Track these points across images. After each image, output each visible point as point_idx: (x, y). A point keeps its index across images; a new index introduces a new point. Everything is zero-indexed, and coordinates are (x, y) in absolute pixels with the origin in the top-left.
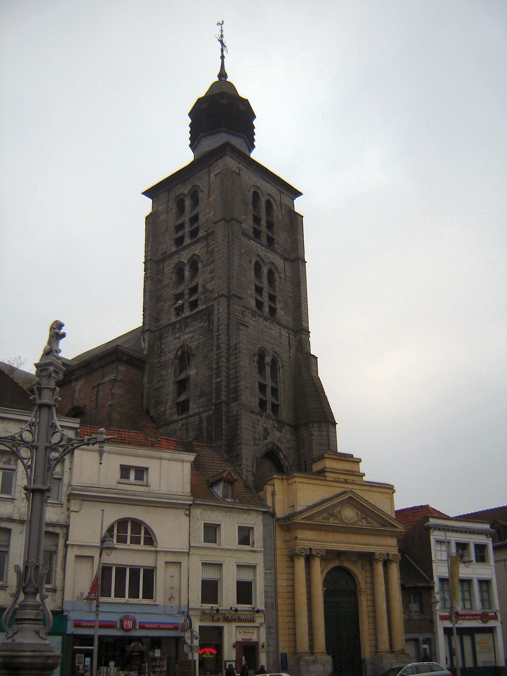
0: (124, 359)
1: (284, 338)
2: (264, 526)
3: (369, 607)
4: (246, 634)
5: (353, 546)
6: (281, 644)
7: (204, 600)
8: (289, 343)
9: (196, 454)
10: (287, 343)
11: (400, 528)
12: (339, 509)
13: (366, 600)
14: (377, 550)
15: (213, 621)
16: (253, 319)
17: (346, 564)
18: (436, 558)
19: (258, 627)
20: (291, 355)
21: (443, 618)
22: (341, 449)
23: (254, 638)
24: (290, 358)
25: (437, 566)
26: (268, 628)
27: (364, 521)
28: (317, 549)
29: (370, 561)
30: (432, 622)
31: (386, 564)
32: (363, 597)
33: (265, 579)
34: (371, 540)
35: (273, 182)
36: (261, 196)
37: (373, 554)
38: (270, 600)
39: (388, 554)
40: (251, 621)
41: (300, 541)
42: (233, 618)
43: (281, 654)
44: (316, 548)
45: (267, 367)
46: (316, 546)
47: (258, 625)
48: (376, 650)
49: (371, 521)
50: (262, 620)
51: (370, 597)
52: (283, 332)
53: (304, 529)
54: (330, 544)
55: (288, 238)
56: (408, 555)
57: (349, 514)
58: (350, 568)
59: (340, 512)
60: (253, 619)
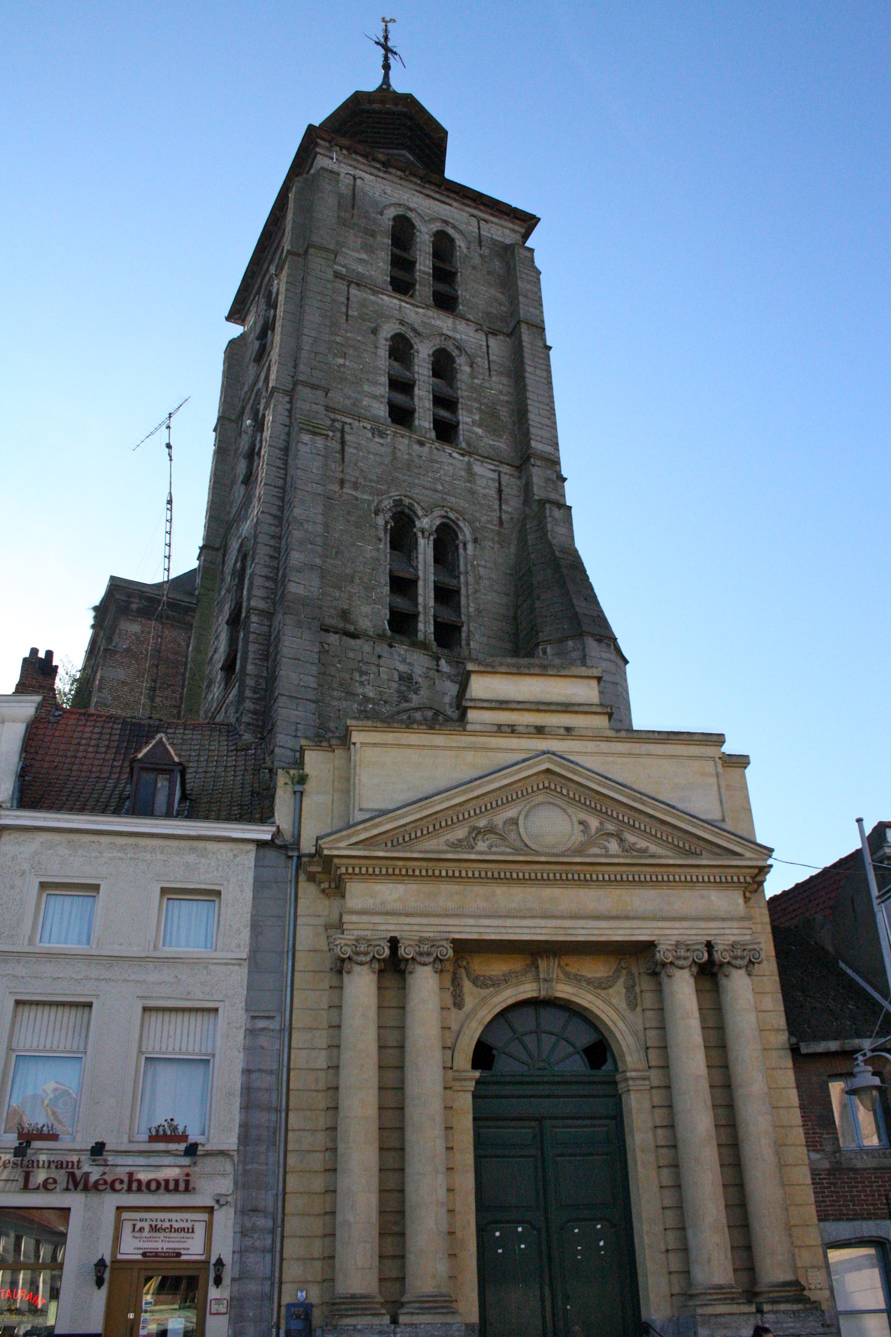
0: (134, 606)
1: (481, 482)
2: (259, 885)
3: (660, 1131)
4: (161, 1235)
5: (567, 923)
6: (292, 1271)
8: (500, 491)
9: (38, 698)
10: (493, 493)
11: (748, 854)
12: (511, 813)
13: (647, 1105)
14: (666, 935)
15: (26, 1187)
16: (377, 439)
19: (210, 1210)
20: (504, 516)
23: (193, 1248)
24: (501, 523)
26: (247, 1210)
27: (613, 846)
28: (422, 941)
29: (655, 974)
31: (709, 972)
32: (633, 1096)
33: (250, 1050)
34: (643, 899)
35: (455, 200)
36: (417, 222)
37: (651, 946)
38: (263, 1118)
39: (709, 945)
40: (176, 1190)
41: (355, 918)
42: (109, 1178)
43: (289, 1306)
44: (416, 936)
45: (421, 541)
47: (209, 1202)
48: (687, 1294)
49: (642, 844)
50: (225, 1185)
51: (658, 1097)
52: (478, 469)
53: (373, 876)
54: (471, 921)
55: (499, 295)
56: (847, 963)
57: (553, 827)
59: (514, 822)
60: (187, 1182)
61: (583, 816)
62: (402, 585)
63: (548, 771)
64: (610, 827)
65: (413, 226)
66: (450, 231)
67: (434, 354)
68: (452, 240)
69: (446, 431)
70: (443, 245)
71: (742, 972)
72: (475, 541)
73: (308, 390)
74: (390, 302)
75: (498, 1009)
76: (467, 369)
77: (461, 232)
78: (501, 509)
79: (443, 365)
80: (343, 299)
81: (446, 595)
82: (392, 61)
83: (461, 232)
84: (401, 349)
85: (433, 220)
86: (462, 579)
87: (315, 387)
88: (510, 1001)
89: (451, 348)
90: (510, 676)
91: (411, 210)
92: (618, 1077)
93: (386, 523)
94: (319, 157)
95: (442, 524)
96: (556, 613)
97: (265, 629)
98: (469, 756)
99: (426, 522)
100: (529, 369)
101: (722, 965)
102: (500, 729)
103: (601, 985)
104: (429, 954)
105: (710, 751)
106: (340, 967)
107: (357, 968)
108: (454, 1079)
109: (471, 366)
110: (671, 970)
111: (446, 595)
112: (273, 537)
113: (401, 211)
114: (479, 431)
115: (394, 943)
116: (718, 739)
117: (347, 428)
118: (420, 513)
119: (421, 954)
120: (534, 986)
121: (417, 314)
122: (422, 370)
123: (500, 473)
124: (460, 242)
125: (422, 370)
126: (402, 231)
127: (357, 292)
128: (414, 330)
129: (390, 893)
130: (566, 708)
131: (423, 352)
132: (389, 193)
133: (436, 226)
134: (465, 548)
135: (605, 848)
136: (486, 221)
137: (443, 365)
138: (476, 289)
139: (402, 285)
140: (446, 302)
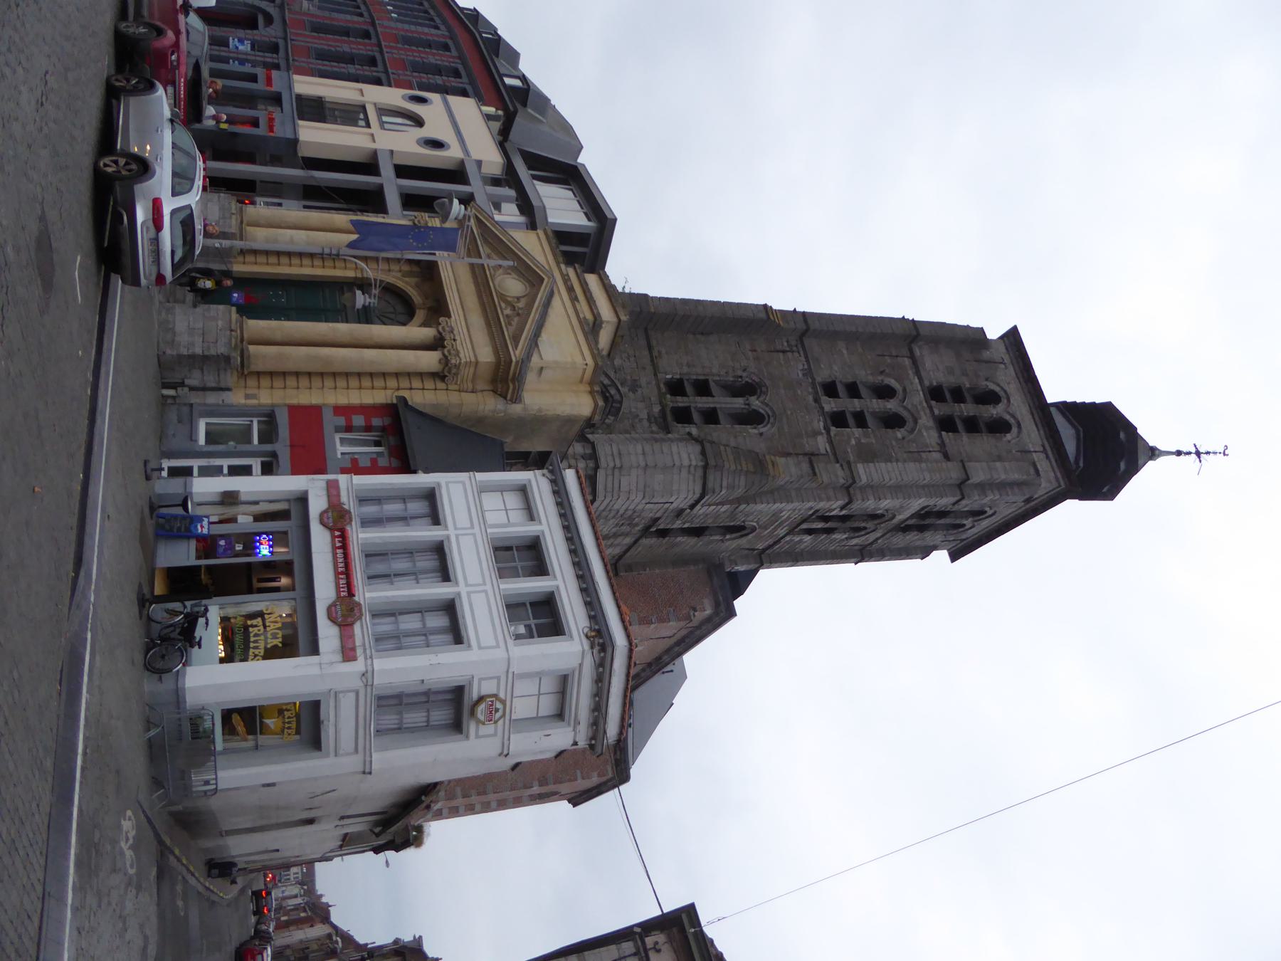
69: (838, 420)
76: (899, 435)
99: (755, 403)
124: (1009, 436)
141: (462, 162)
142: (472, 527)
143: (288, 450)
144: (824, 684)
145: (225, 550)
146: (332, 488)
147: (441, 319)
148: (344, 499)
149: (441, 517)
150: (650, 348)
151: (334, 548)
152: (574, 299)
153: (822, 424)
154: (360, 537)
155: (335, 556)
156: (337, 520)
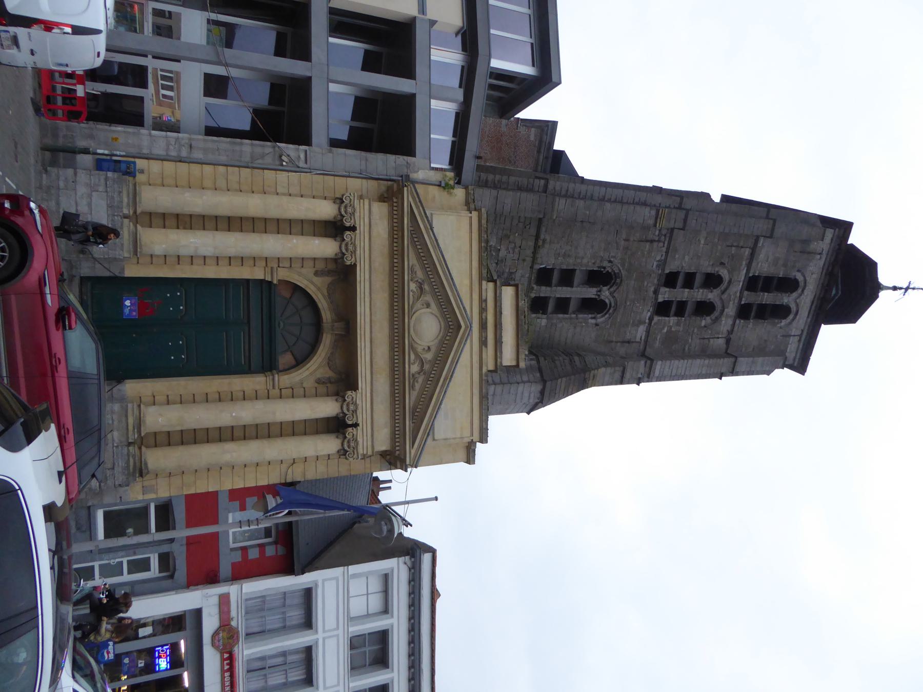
7: (191, 499)
11: (413, 451)
13: (258, 387)
17: (327, 340)
18: (355, 576)
21: (224, 601)
22: (495, 422)
25: (337, 579)
30: (212, 579)
31: (337, 426)
34: (383, 385)
36: (795, 295)
37: (355, 388)
39: (356, 425)
41: (367, 207)
46: (361, 240)
49: (417, 386)
58: (315, 358)
59: (428, 306)
61: (433, 349)
62: (567, 277)
63: (460, 327)
64: (427, 367)
65: (792, 292)
66: (791, 317)
67: (711, 303)
68: (785, 317)
69: (662, 309)
70: (781, 312)
71: (340, 447)
72: (597, 325)
73: (683, 217)
74: (741, 276)
75: (314, 296)
76: (703, 323)
77: (790, 323)
78: (617, 342)
79: (704, 308)
80: (741, 244)
81: (562, 305)
82: (899, 292)
83: (790, 323)
84: (712, 281)
85: (797, 305)
86: (574, 316)
87: (685, 220)
88: (320, 305)
89: (716, 314)
90: (514, 307)
91: (803, 291)
92: (274, 371)
93: (604, 268)
94: (832, 231)
95: (606, 304)
96: (551, 373)
97: (537, 189)
98: (467, 282)
99: (606, 294)
100: (707, 361)
101: (344, 434)
102: (483, 301)
103: (330, 362)
104: (347, 250)
105: (476, 437)
106: (339, 201)
107: (337, 206)
108: (272, 268)
109: (705, 326)
110: (340, 399)
111: (562, 305)
112: (592, 195)
113: (802, 284)
114: (665, 330)
115: (353, 229)
116: (484, 439)
117: (661, 244)
118: (612, 290)
119: (347, 245)
120: (330, 320)
121: (734, 293)
122: (700, 294)
123: (640, 343)
124: (784, 322)
125: (700, 294)
126: (788, 285)
127: (747, 253)
128: (726, 289)
129: (381, 229)
130: (498, 342)
131: (711, 296)
132: (812, 275)
133: (793, 307)
134: (592, 318)
135: (414, 363)
136: (799, 341)
137: (704, 308)
138: (754, 332)
139: (753, 284)
140: (744, 312)
141: (414, 20)
142: (338, 628)
143: (184, 548)
144: (555, 506)
145: (129, 668)
146: (224, 601)
147: (349, 393)
148: (233, 613)
149: (314, 620)
150: (537, 237)
151: (223, 671)
152: (483, 343)
153: (649, 314)
154: (245, 652)
155: (223, 678)
156: (227, 638)
